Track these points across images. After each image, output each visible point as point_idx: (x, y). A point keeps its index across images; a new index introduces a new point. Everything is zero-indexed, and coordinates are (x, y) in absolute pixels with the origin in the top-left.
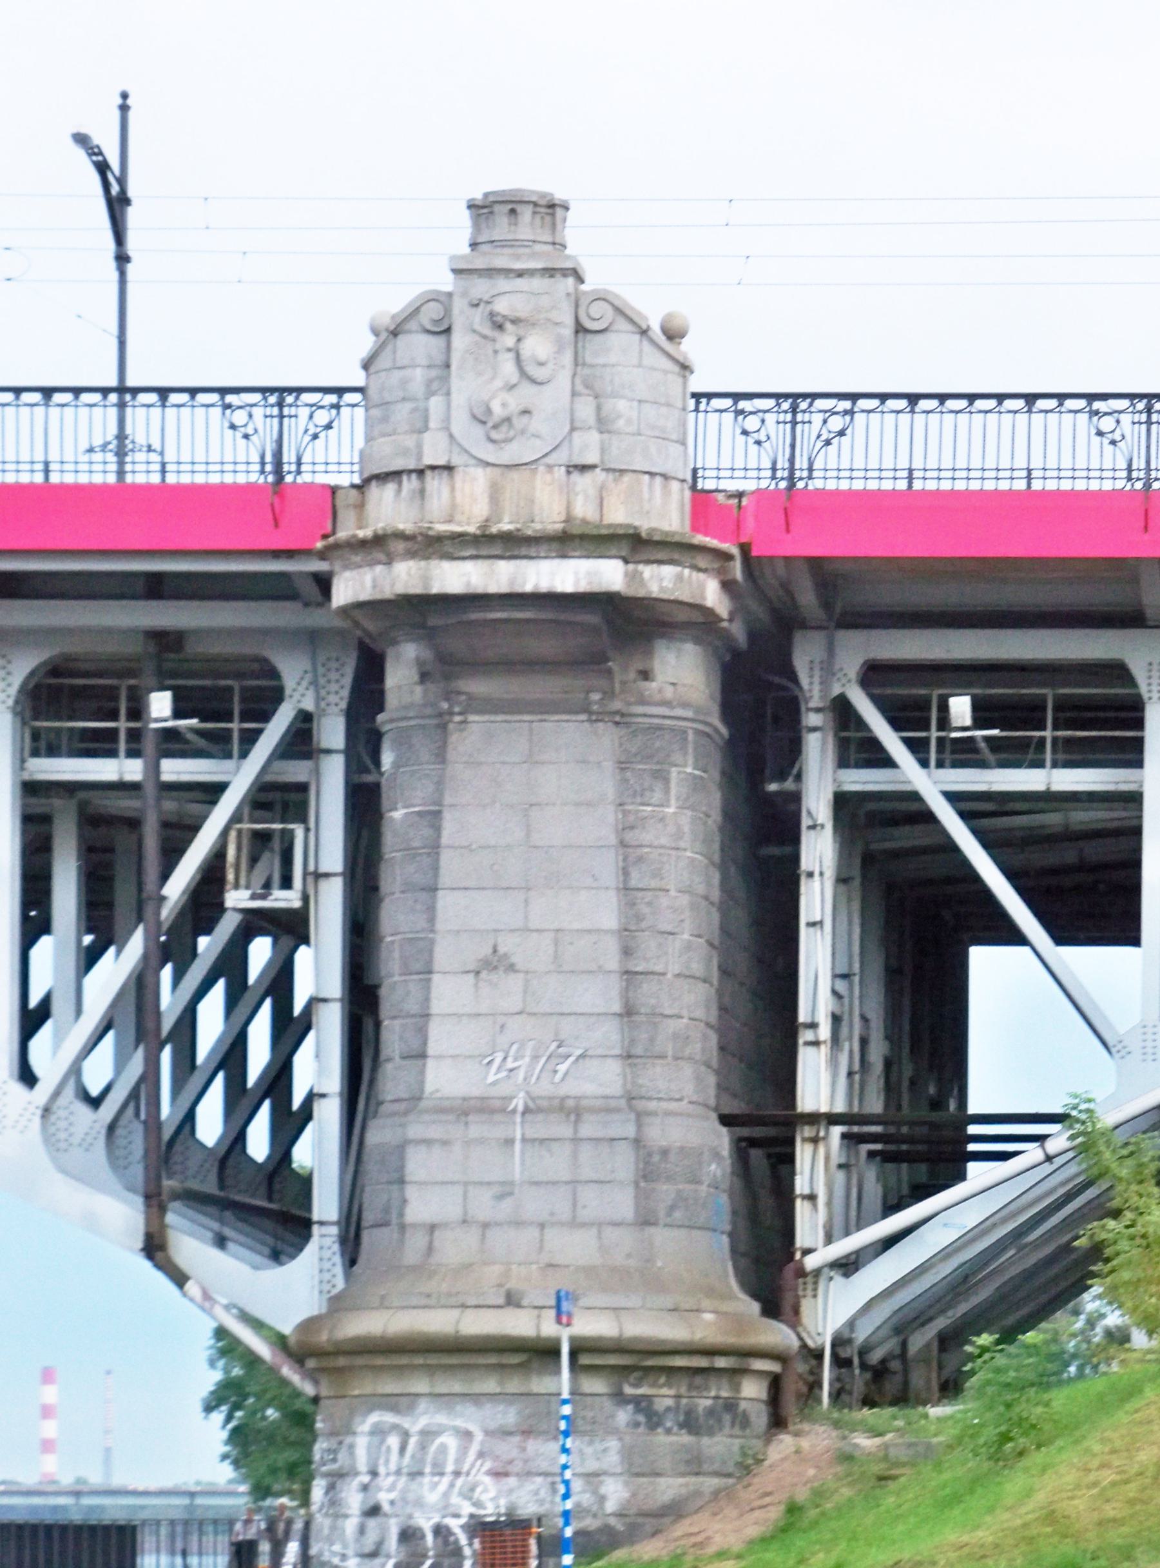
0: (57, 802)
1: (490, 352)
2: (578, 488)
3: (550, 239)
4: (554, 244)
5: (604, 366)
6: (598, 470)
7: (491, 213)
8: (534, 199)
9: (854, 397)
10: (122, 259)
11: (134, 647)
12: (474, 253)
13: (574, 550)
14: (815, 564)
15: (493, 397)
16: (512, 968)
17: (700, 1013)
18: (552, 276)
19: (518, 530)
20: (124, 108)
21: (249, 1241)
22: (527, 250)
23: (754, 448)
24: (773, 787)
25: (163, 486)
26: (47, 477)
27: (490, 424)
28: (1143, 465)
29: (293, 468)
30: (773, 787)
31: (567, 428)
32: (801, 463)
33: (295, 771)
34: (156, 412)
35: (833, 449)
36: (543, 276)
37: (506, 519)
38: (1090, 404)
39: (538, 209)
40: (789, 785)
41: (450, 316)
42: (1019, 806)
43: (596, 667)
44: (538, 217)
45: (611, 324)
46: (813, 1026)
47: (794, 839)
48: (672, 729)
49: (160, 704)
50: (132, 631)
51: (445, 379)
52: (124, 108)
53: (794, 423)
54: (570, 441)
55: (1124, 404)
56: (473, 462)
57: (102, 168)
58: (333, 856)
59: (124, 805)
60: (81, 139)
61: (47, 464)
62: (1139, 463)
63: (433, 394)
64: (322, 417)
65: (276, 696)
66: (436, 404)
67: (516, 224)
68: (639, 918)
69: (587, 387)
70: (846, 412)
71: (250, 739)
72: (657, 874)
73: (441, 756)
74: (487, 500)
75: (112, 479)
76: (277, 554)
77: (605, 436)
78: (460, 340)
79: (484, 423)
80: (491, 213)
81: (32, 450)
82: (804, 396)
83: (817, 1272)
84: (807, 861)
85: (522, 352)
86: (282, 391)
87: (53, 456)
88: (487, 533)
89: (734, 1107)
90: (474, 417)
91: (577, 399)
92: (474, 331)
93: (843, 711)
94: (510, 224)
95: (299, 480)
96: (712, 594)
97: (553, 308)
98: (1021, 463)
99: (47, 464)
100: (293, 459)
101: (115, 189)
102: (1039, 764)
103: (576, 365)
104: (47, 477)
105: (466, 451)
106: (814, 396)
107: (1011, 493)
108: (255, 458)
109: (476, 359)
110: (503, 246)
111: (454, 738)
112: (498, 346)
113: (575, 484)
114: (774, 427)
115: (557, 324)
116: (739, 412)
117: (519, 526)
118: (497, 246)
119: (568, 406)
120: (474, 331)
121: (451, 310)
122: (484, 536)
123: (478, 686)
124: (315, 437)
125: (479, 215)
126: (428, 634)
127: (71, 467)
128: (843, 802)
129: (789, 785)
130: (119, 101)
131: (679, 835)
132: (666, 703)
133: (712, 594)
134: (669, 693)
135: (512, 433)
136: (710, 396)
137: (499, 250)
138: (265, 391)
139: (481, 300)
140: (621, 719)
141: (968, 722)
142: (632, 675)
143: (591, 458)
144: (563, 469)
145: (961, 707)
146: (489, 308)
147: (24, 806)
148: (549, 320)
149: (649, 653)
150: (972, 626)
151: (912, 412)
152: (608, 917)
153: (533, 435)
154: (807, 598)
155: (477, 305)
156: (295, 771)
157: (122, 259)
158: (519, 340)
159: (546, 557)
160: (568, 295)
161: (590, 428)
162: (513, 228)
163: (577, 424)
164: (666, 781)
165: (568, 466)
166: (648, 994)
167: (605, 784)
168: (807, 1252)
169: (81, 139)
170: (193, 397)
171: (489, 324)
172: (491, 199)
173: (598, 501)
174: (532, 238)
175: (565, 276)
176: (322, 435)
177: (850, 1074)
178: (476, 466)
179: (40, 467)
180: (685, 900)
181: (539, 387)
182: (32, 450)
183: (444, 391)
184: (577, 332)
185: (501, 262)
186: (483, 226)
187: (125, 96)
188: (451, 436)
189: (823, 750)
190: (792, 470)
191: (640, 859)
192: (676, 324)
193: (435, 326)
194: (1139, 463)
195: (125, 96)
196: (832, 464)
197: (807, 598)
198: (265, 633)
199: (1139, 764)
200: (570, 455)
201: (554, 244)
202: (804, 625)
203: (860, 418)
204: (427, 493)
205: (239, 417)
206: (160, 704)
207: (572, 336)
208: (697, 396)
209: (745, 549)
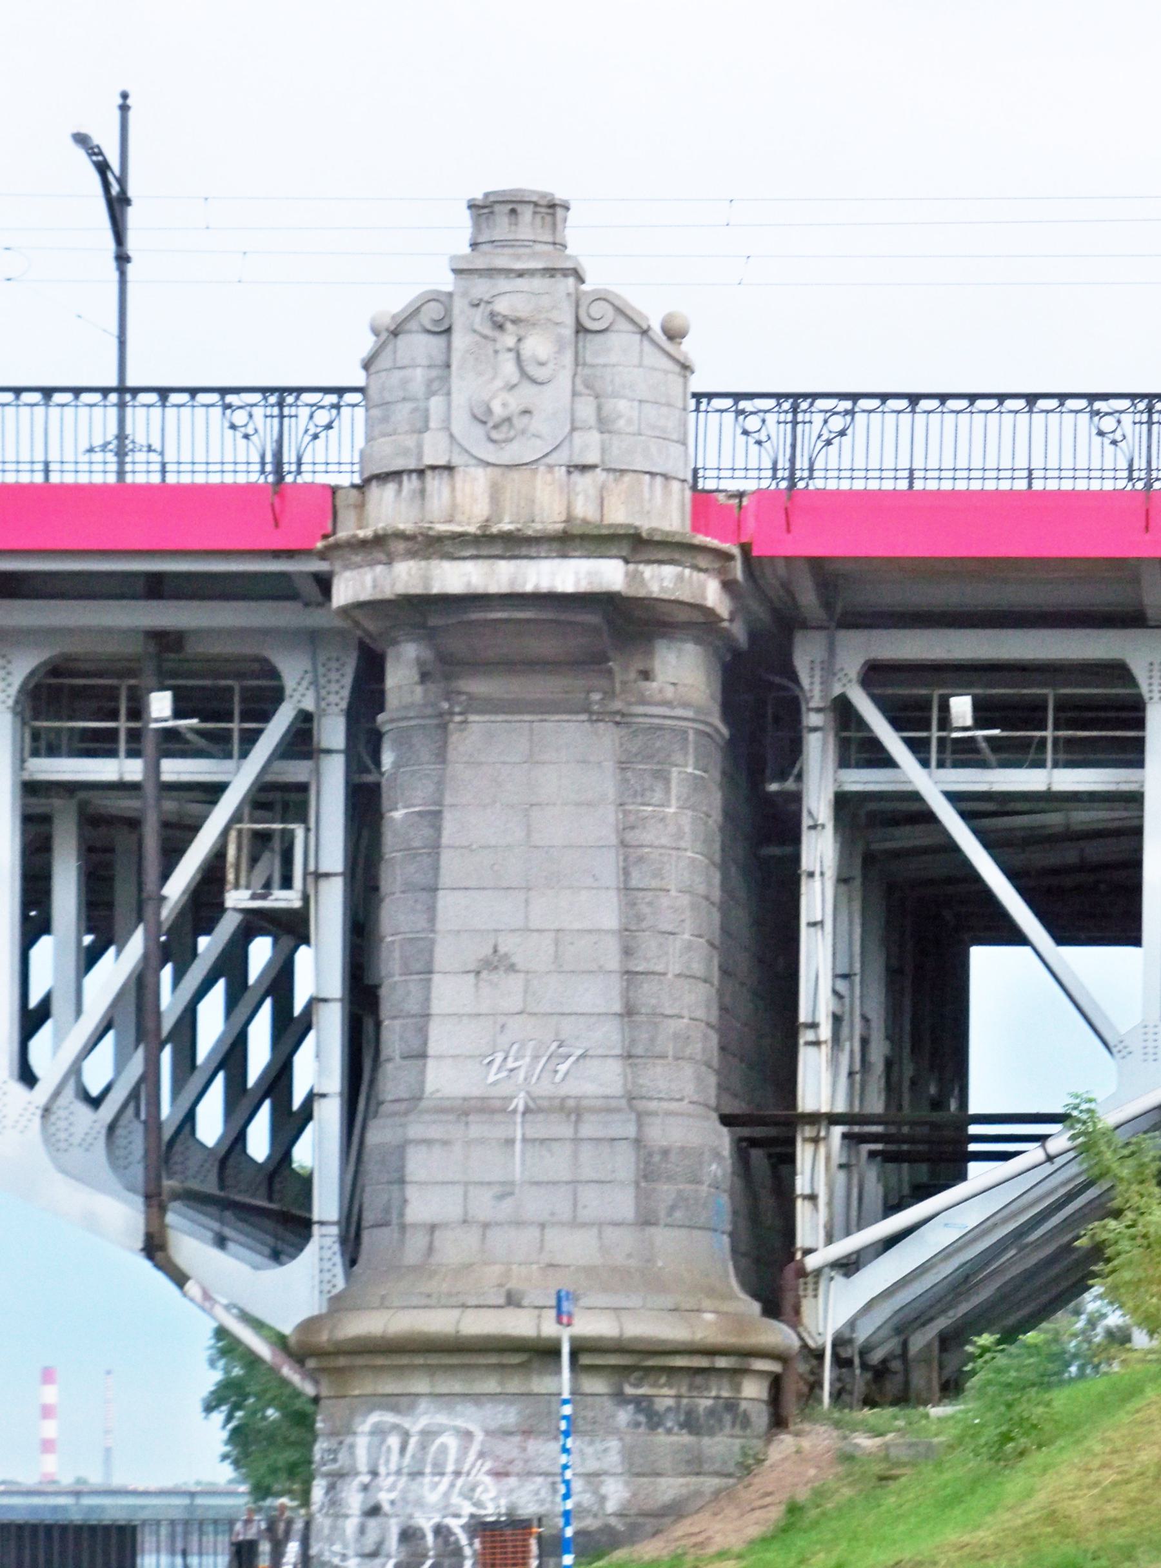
0: (57, 802)
1: (491, 352)
2: (579, 488)
3: (550, 239)
4: (554, 244)
5: (605, 366)
6: (598, 470)
7: (492, 213)
8: (534, 199)
9: (855, 397)
10: (122, 259)
11: (135, 647)
12: (475, 253)
13: (575, 550)
14: (816, 564)
15: (493, 397)
16: (512, 968)
17: (700, 1013)
18: (552, 276)
19: (519, 530)
20: (124, 108)
21: (249, 1241)
22: (527, 250)
23: (754, 448)
24: (774, 787)
25: (163, 486)
26: (47, 477)
27: (491, 424)
28: (1144, 465)
29: (294, 468)
30: (774, 787)
31: (567, 428)
32: (802, 463)
33: (295, 771)
34: (156, 412)
35: (833, 449)
36: (543, 276)
37: (507, 519)
38: (1091, 404)
39: (539, 209)
40: (790, 785)
41: (451, 316)
42: (1019, 806)
43: (596, 667)
44: (538, 217)
45: (611, 324)
46: (814, 1026)
47: (795, 839)
48: (672, 729)
49: (160, 704)
50: (133, 631)
51: (445, 379)
52: (124, 108)
53: (795, 423)
54: (571, 441)
55: (1125, 404)
56: (473, 462)
57: (103, 168)
58: (333, 856)
59: (124, 805)
60: (81, 139)
61: (47, 464)
62: (1140, 463)
63: (434, 394)
64: (322, 417)
65: (277, 696)
66: (436, 404)
67: (516, 224)
68: (640, 918)
69: (587, 387)
70: (847, 412)
71: (250, 739)
72: (658, 874)
73: (441, 756)
74: (487, 500)
75: (112, 479)
76: (277, 554)
77: (606, 436)
78: (460, 340)
79: (484, 423)
80: (492, 213)
81: (32, 450)
82: (805, 396)
83: (818, 1272)
84: (808, 861)
85: (522, 352)
86: (283, 391)
87: (54, 456)
88: (488, 533)
89: (735, 1107)
90: (475, 417)
91: (577, 399)
92: (475, 331)
93: (844, 711)
94: (510, 224)
95: (300, 480)
96: (712, 594)
97: (553, 308)
98: (1022, 463)
99: (47, 464)
100: (294, 459)
101: (115, 189)
102: (1039, 764)
103: (577, 365)
104: (47, 477)
105: (467, 451)
106: (815, 396)
107: (1011, 493)
108: (256, 458)
109: (477, 359)
110: (504, 246)
111: (454, 738)
112: (498, 346)
113: (575, 484)
114: (775, 427)
115: (557, 324)
116: (740, 412)
117: (519, 526)
118: (497, 246)
119: (568, 406)
120: (475, 331)
121: (451, 310)
122: (484, 536)
123: (478, 686)
124: (316, 437)
125: (480, 215)
126: (429, 634)
127: (71, 467)
128: (843, 802)
129: (790, 785)
130: (120, 101)
131: (679, 835)
132: (667, 703)
133: (712, 594)
134: (670, 693)
135: (512, 433)
136: (710, 396)
137: (499, 250)
138: (265, 391)
139: (481, 300)
140: (621, 719)
141: (969, 722)
142: (633, 675)
143: (592, 458)
144: (564, 469)
145: (962, 707)
146: (489, 308)
147: (24, 806)
148: (549, 320)
149: (649, 653)
150: (973, 626)
151: (913, 412)
152: (609, 917)
153: (534, 435)
154: (808, 598)
155: (477, 305)
156: (295, 771)
157: (122, 259)
158: (519, 340)
159: (546, 557)
160: (569, 295)
161: (590, 428)
162: (513, 228)
163: (578, 424)
164: (667, 781)
165: (569, 466)
166: (649, 994)
167: (606, 784)
168: (808, 1252)
169: (81, 139)
170: (193, 397)
171: (489, 324)
172: (492, 199)
173: (598, 501)
174: (532, 238)
175: (565, 276)
176: (323, 435)
177: (851, 1074)
178: (477, 466)
179: (40, 467)
180: (685, 900)
181: (540, 387)
182: (32, 450)
183: (444, 391)
184: (577, 332)
185: (501, 262)
186: (484, 226)
187: (125, 96)
188: (452, 436)
189: (824, 750)
190: (793, 470)
191: (641, 859)
192: (677, 324)
193: (435, 326)
194: (1140, 463)
195: (125, 96)
196: (833, 464)
197: (808, 598)
198: (265, 633)
199: (1140, 764)
200: (571, 455)
201: (554, 244)
202: (805, 625)
203: (860, 418)
204: (428, 493)
205: (240, 417)
206: (160, 704)
207: (573, 336)
208: (697, 396)
209: (746, 549)
